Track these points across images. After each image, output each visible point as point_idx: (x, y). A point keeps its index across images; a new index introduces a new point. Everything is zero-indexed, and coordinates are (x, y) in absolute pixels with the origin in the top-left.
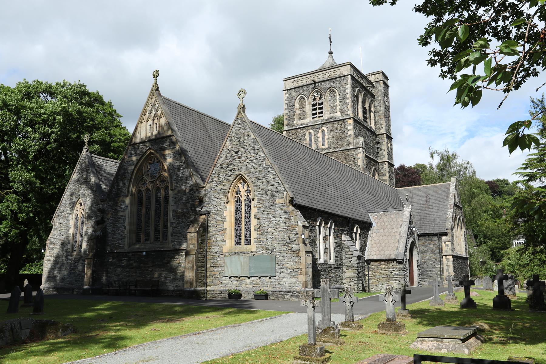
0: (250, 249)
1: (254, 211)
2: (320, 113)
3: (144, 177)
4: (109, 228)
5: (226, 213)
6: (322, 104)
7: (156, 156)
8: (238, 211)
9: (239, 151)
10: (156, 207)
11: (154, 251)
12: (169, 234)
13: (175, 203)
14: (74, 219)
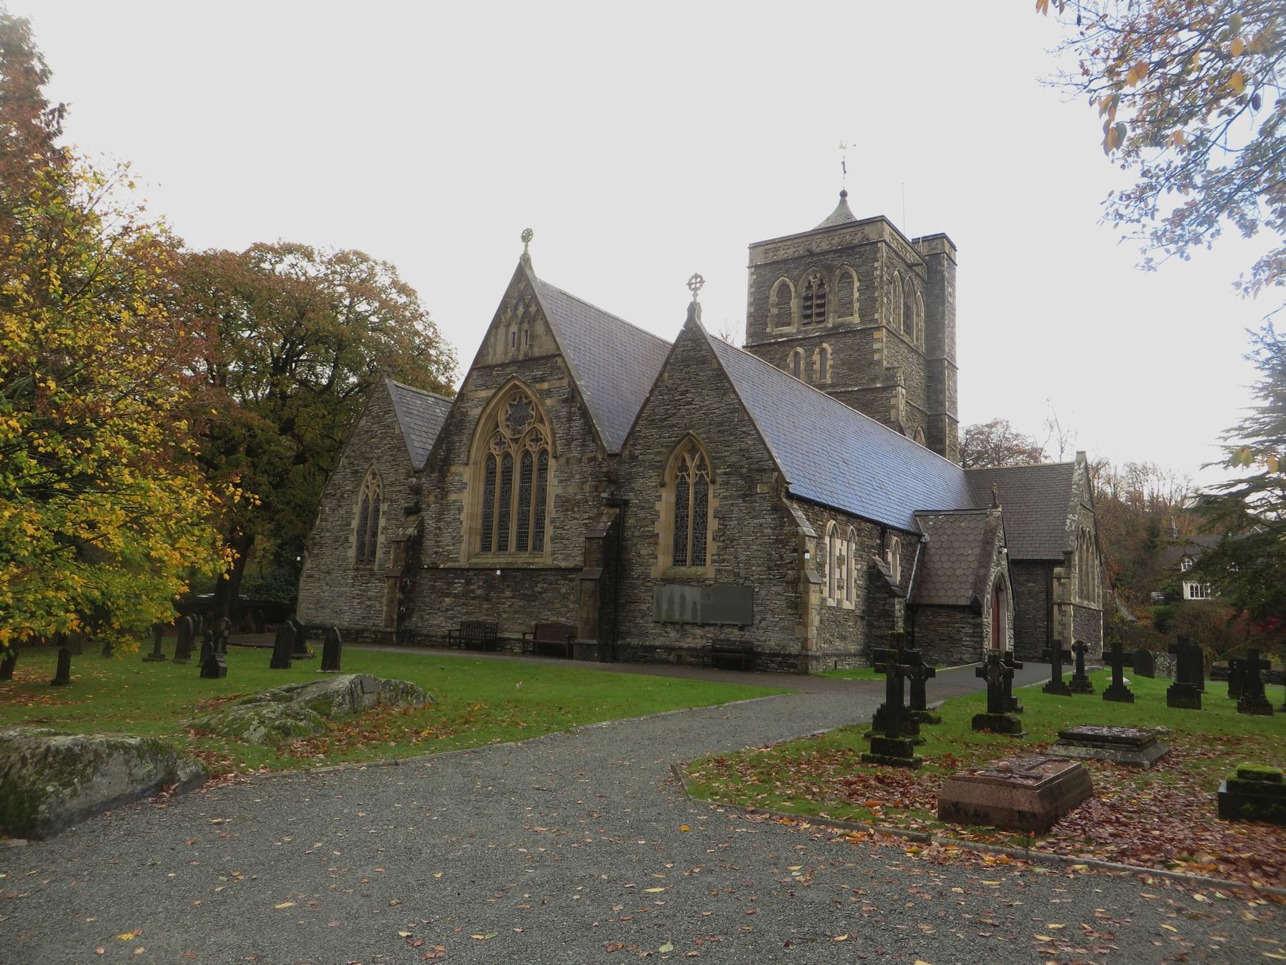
0: (705, 574)
1: (713, 503)
2: (819, 315)
3: (500, 429)
4: (430, 524)
5: (659, 506)
6: (823, 296)
7: (525, 393)
8: (681, 503)
9: (687, 391)
10: (521, 487)
11: (518, 570)
12: (547, 539)
13: (561, 481)
14: (360, 503)
